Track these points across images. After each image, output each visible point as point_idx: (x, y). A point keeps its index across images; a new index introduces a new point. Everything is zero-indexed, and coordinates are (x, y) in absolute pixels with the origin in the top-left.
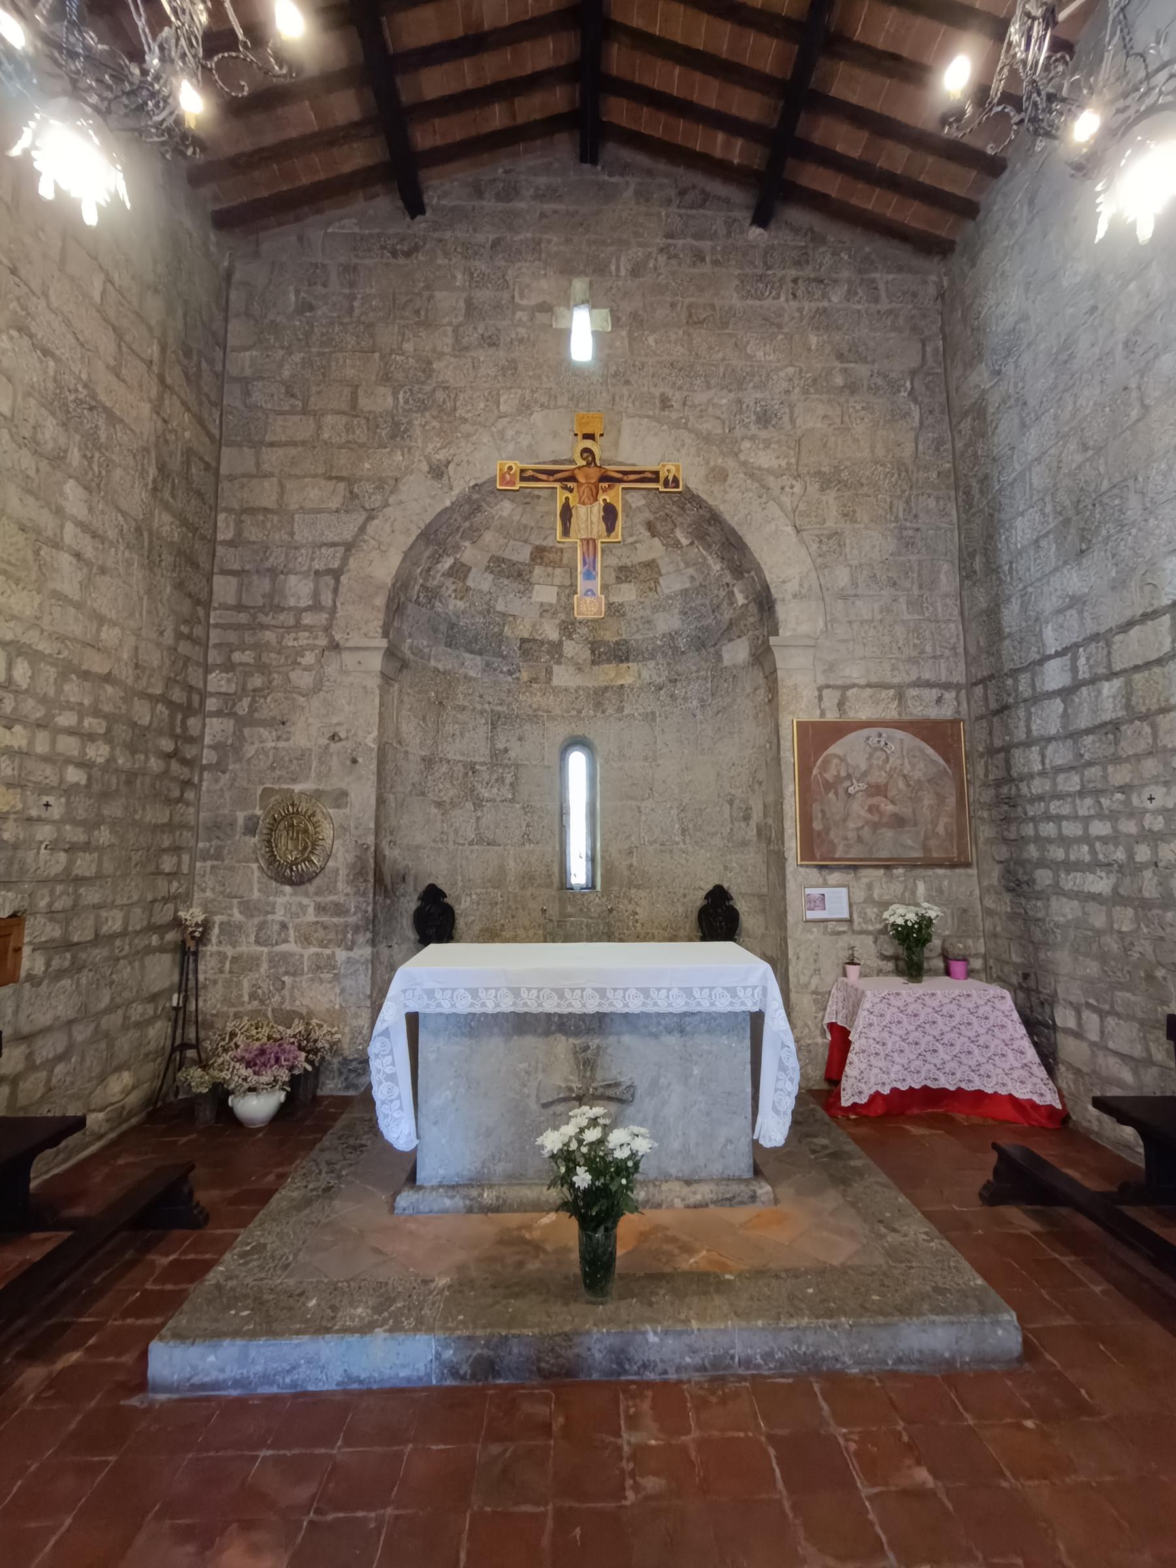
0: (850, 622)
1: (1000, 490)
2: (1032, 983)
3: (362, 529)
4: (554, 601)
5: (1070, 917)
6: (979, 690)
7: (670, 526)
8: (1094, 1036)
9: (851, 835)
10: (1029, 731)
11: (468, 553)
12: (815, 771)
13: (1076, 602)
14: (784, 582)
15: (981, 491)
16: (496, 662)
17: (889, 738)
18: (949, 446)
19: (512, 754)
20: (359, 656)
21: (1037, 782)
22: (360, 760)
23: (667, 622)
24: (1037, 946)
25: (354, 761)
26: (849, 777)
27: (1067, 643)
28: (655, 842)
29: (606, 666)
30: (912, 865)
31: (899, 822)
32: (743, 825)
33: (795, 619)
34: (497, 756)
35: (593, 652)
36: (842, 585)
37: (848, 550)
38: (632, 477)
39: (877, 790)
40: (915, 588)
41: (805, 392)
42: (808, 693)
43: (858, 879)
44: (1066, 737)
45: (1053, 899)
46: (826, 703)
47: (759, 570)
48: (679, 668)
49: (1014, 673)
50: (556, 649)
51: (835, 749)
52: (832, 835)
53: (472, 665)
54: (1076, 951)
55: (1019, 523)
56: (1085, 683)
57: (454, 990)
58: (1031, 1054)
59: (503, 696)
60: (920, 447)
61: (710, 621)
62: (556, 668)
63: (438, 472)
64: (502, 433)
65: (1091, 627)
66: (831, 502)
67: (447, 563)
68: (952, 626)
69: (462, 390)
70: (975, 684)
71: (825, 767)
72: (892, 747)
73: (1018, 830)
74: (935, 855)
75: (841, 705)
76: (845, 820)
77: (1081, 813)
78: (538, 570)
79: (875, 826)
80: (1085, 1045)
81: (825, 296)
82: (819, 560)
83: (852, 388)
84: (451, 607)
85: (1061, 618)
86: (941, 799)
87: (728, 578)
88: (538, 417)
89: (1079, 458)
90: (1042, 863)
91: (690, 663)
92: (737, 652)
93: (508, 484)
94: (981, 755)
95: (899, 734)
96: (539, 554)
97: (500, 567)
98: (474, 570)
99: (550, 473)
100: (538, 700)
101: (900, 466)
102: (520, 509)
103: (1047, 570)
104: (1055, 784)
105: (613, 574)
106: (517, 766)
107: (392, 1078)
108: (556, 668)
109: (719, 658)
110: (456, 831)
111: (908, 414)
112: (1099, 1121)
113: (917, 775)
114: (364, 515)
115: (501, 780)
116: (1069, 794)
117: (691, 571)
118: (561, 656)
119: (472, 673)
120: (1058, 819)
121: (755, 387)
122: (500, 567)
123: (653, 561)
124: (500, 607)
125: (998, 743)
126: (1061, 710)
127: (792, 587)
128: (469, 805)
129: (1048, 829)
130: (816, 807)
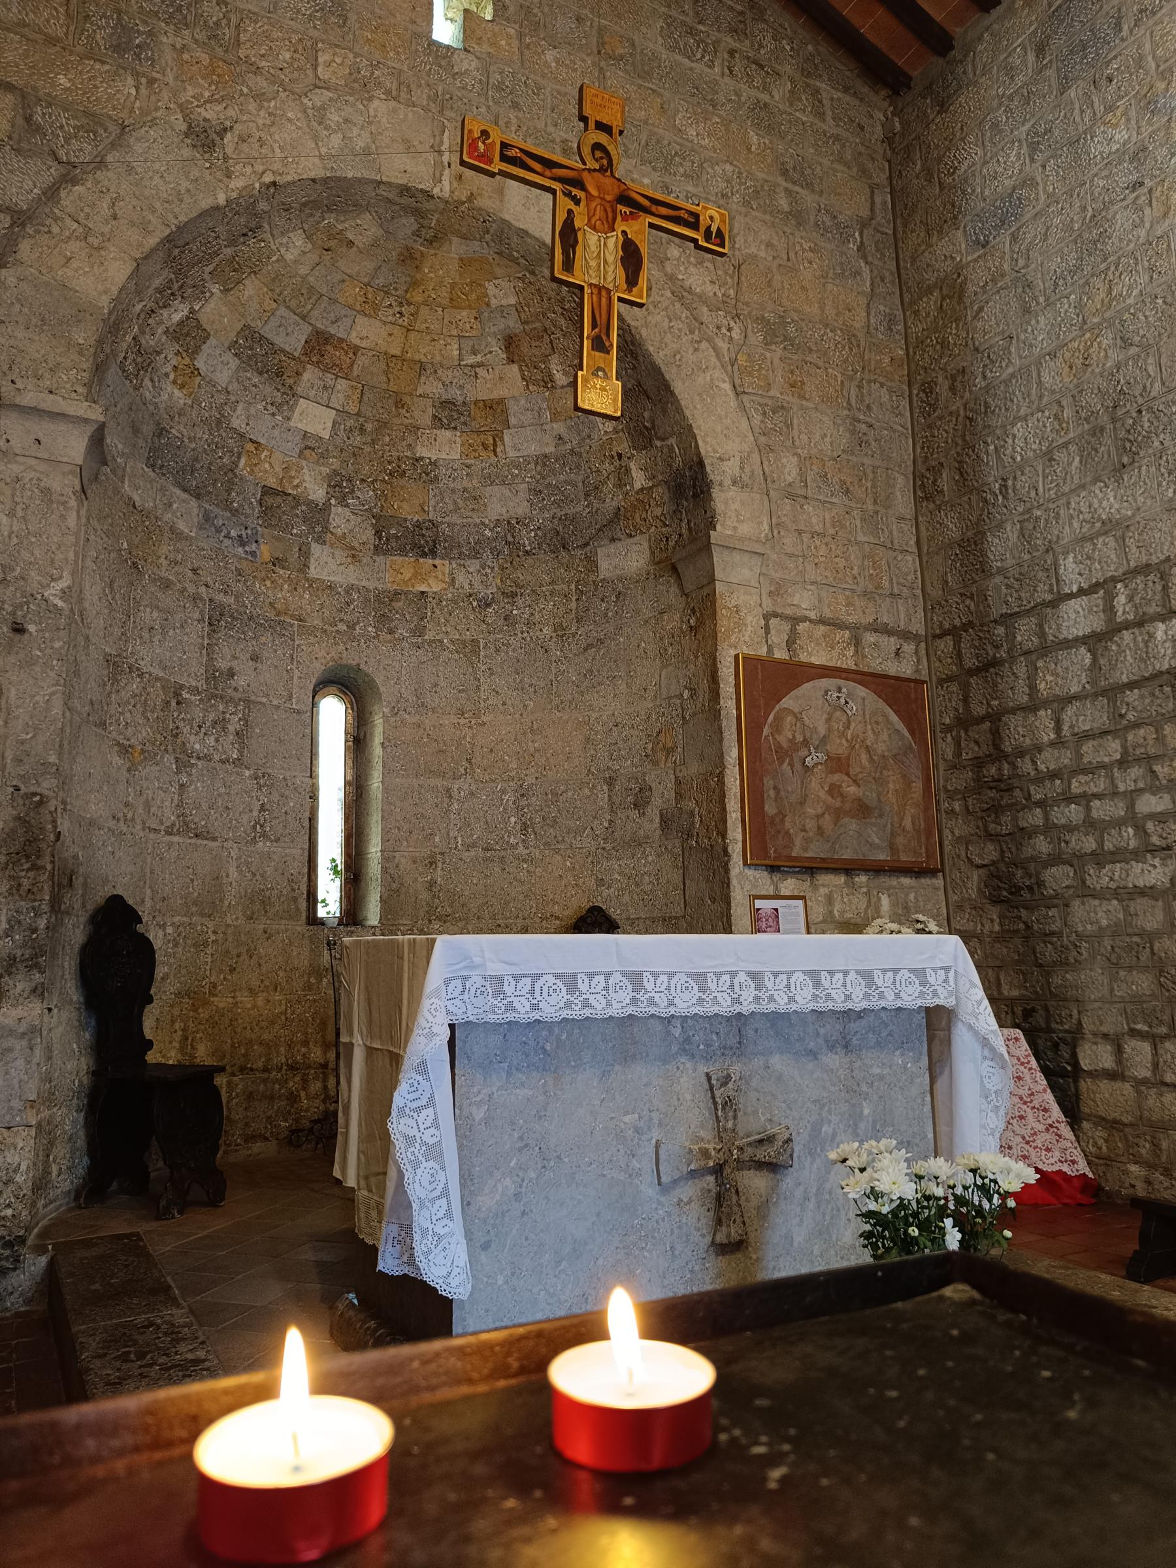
0: (800, 532)
1: (987, 389)
2: (1039, 1019)
3: (51, 194)
4: (326, 435)
5: (1104, 922)
6: (946, 645)
7: (545, 347)
8: (1144, 1073)
9: (810, 824)
10: (1033, 688)
11: (215, 310)
12: (766, 731)
13: (1115, 527)
14: (721, 459)
15: (952, 389)
16: (221, 516)
17: (849, 694)
18: (900, 327)
19: (241, 681)
20: (42, 428)
21: (1047, 754)
22: (32, 628)
23: (505, 503)
24: (1046, 970)
25: (19, 629)
26: (806, 743)
27: (1098, 576)
28: (474, 845)
29: (399, 559)
30: (876, 869)
31: (863, 810)
32: (634, 814)
33: (736, 513)
34: (218, 681)
35: (378, 533)
36: (790, 479)
37: (796, 433)
38: (663, 211)
39: (838, 764)
40: (869, 501)
41: (747, 204)
42: (754, 621)
43: (815, 888)
44: (1096, 695)
45: (1076, 903)
46: (774, 638)
47: (687, 433)
48: (519, 575)
49: (1008, 619)
50: (318, 515)
51: (787, 702)
52: (788, 825)
53: (184, 513)
54: (1114, 965)
55: (1019, 429)
56: (1127, 625)
57: (536, 977)
58: (1056, 1112)
59: (230, 578)
60: (873, 321)
61: (580, 508)
62: (316, 549)
63: (205, 138)
64: (321, 111)
65: (1136, 557)
66: (776, 361)
67: (177, 314)
68: (909, 558)
69: (254, 17)
70: (940, 636)
71: (777, 728)
72: (854, 707)
73: (1015, 819)
74: (903, 858)
75: (790, 643)
76: (802, 803)
77: (1122, 787)
78: (310, 375)
79: (838, 814)
80: (1128, 1088)
81: (765, 88)
82: (762, 439)
83: (797, 217)
84: (164, 397)
85: (1088, 547)
86: (907, 782)
87: (623, 447)
88: (379, 107)
89: (1115, 356)
90: (1056, 859)
91: (538, 571)
92: (627, 558)
93: (480, 157)
94: (948, 729)
95: (861, 691)
96: (320, 345)
97: (253, 349)
98: (212, 341)
99: (549, 164)
100: (284, 594)
101: (851, 337)
102: (314, 257)
103: (1066, 489)
104: (1080, 756)
105: (430, 411)
106: (247, 701)
107: (434, 1152)
108: (316, 549)
109: (591, 563)
110: (147, 806)
111: (858, 273)
112: (1149, 1182)
113: (881, 748)
114: (55, 171)
115: (221, 723)
116: (1104, 766)
117: (559, 428)
118: (326, 529)
119: (181, 526)
120: (1085, 799)
121: (685, 175)
122: (253, 349)
123: (501, 401)
124: (238, 422)
125: (979, 710)
126: (1088, 661)
127: (731, 468)
128: (169, 760)
129: (1073, 813)
130: (768, 782)
